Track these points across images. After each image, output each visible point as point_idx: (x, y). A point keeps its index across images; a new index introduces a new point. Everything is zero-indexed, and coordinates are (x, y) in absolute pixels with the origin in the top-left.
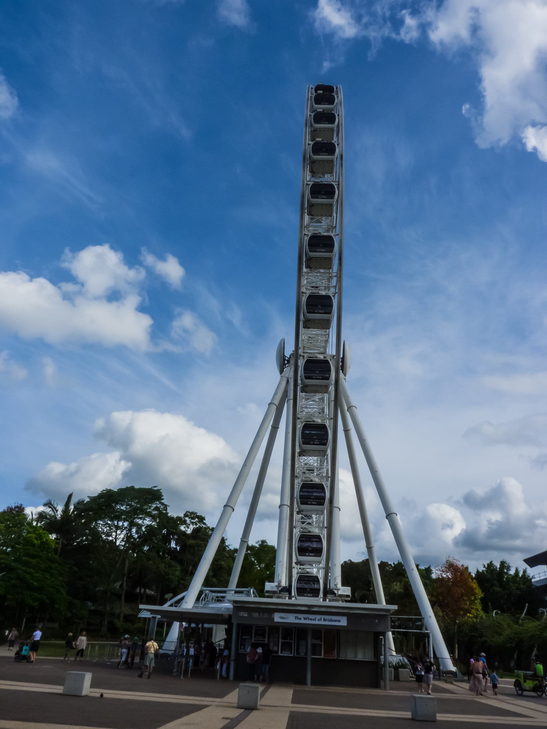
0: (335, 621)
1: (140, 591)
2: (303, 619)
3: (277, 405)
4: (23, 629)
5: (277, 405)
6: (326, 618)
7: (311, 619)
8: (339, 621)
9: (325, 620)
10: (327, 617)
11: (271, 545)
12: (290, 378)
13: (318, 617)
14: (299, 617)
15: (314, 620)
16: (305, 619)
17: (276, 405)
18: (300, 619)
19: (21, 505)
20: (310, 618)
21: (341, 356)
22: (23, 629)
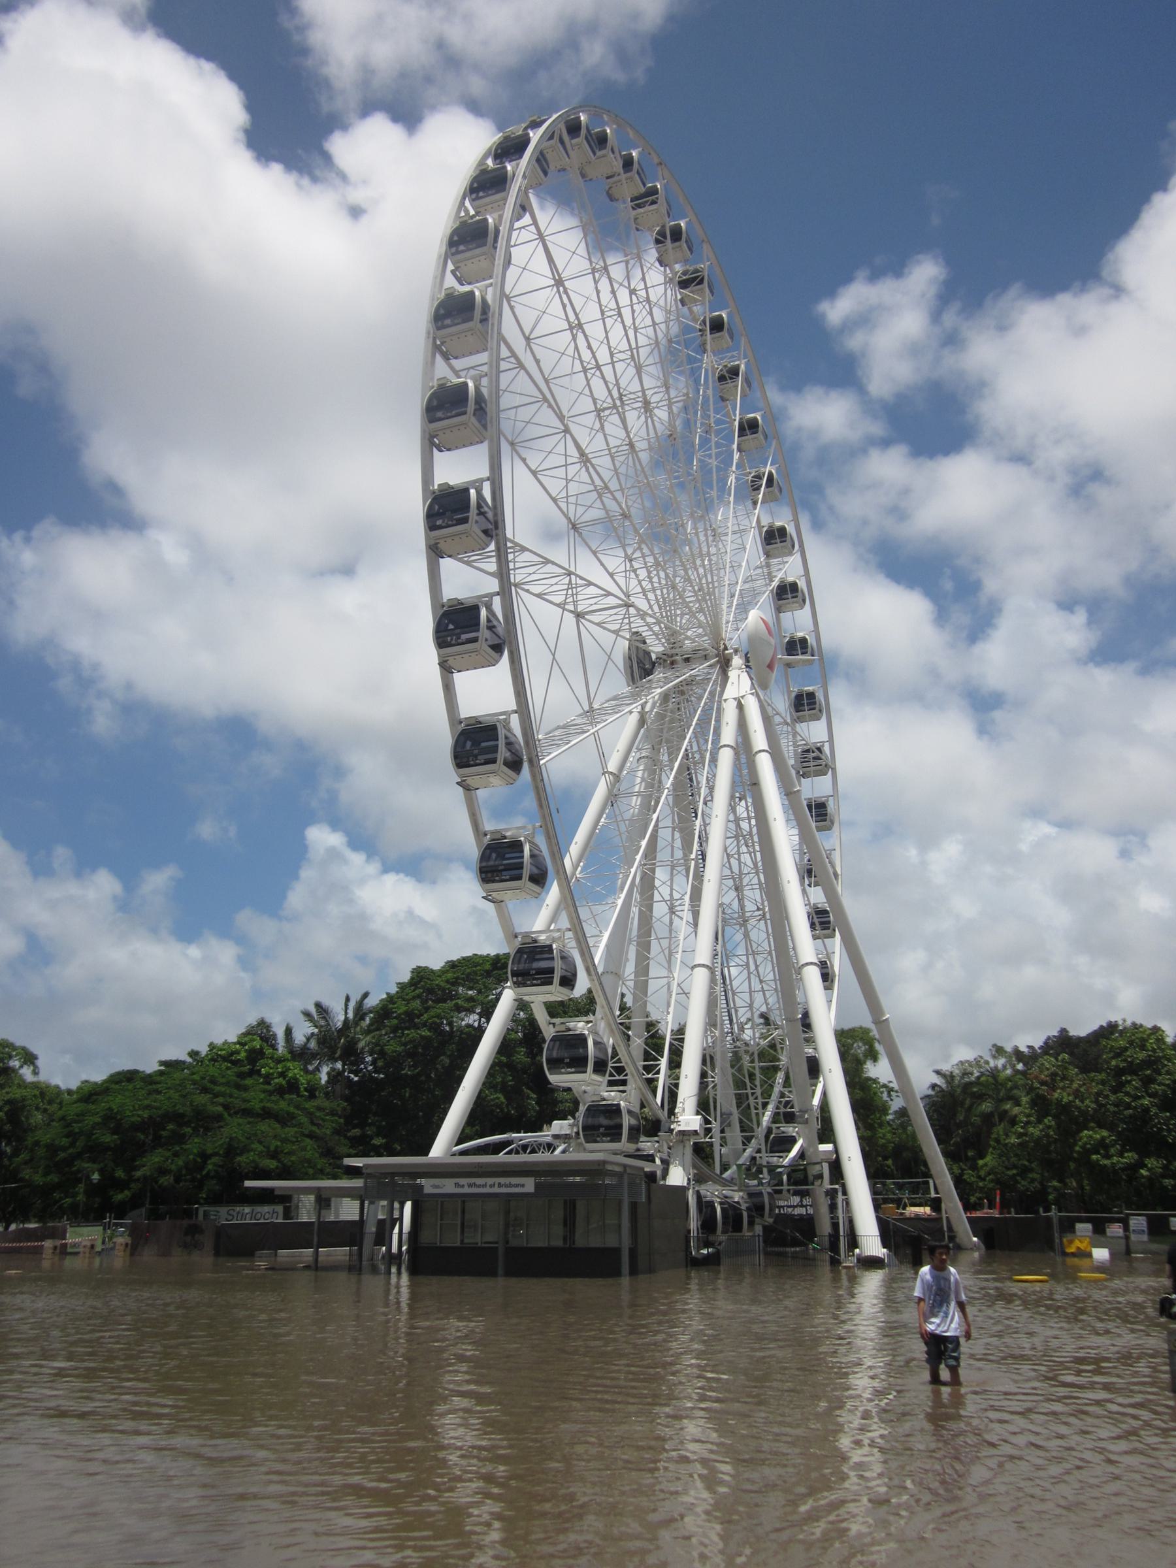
0: (517, 1186)
1: (1165, 1372)
2: (466, 1186)
3: (767, 748)
4: (227, 1398)
5: (767, 748)
6: (503, 1183)
7: (479, 1186)
8: (523, 1186)
9: (500, 1185)
10: (502, 1180)
11: (442, 964)
12: (742, 697)
13: (490, 1181)
14: (461, 1184)
15: (484, 1186)
16: (470, 1185)
17: (767, 751)
18: (463, 1186)
19: (1063, 1031)
20: (477, 1183)
21: (642, 730)
22: (227, 1398)
